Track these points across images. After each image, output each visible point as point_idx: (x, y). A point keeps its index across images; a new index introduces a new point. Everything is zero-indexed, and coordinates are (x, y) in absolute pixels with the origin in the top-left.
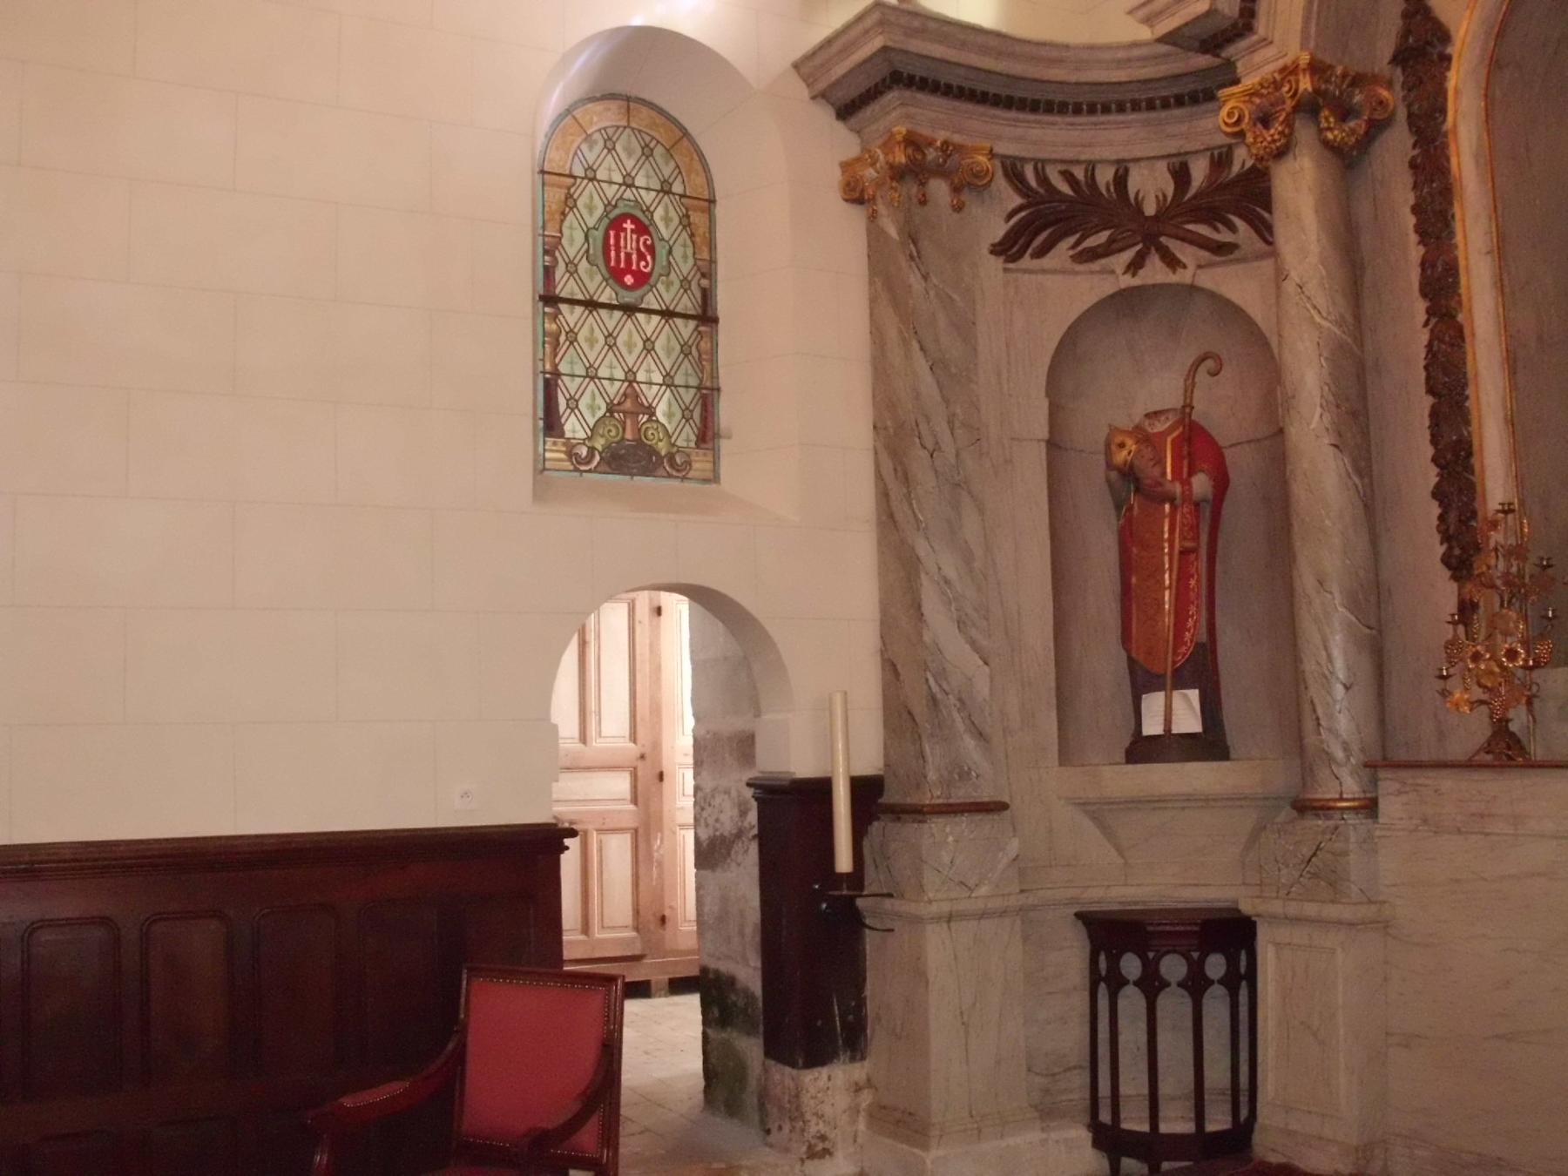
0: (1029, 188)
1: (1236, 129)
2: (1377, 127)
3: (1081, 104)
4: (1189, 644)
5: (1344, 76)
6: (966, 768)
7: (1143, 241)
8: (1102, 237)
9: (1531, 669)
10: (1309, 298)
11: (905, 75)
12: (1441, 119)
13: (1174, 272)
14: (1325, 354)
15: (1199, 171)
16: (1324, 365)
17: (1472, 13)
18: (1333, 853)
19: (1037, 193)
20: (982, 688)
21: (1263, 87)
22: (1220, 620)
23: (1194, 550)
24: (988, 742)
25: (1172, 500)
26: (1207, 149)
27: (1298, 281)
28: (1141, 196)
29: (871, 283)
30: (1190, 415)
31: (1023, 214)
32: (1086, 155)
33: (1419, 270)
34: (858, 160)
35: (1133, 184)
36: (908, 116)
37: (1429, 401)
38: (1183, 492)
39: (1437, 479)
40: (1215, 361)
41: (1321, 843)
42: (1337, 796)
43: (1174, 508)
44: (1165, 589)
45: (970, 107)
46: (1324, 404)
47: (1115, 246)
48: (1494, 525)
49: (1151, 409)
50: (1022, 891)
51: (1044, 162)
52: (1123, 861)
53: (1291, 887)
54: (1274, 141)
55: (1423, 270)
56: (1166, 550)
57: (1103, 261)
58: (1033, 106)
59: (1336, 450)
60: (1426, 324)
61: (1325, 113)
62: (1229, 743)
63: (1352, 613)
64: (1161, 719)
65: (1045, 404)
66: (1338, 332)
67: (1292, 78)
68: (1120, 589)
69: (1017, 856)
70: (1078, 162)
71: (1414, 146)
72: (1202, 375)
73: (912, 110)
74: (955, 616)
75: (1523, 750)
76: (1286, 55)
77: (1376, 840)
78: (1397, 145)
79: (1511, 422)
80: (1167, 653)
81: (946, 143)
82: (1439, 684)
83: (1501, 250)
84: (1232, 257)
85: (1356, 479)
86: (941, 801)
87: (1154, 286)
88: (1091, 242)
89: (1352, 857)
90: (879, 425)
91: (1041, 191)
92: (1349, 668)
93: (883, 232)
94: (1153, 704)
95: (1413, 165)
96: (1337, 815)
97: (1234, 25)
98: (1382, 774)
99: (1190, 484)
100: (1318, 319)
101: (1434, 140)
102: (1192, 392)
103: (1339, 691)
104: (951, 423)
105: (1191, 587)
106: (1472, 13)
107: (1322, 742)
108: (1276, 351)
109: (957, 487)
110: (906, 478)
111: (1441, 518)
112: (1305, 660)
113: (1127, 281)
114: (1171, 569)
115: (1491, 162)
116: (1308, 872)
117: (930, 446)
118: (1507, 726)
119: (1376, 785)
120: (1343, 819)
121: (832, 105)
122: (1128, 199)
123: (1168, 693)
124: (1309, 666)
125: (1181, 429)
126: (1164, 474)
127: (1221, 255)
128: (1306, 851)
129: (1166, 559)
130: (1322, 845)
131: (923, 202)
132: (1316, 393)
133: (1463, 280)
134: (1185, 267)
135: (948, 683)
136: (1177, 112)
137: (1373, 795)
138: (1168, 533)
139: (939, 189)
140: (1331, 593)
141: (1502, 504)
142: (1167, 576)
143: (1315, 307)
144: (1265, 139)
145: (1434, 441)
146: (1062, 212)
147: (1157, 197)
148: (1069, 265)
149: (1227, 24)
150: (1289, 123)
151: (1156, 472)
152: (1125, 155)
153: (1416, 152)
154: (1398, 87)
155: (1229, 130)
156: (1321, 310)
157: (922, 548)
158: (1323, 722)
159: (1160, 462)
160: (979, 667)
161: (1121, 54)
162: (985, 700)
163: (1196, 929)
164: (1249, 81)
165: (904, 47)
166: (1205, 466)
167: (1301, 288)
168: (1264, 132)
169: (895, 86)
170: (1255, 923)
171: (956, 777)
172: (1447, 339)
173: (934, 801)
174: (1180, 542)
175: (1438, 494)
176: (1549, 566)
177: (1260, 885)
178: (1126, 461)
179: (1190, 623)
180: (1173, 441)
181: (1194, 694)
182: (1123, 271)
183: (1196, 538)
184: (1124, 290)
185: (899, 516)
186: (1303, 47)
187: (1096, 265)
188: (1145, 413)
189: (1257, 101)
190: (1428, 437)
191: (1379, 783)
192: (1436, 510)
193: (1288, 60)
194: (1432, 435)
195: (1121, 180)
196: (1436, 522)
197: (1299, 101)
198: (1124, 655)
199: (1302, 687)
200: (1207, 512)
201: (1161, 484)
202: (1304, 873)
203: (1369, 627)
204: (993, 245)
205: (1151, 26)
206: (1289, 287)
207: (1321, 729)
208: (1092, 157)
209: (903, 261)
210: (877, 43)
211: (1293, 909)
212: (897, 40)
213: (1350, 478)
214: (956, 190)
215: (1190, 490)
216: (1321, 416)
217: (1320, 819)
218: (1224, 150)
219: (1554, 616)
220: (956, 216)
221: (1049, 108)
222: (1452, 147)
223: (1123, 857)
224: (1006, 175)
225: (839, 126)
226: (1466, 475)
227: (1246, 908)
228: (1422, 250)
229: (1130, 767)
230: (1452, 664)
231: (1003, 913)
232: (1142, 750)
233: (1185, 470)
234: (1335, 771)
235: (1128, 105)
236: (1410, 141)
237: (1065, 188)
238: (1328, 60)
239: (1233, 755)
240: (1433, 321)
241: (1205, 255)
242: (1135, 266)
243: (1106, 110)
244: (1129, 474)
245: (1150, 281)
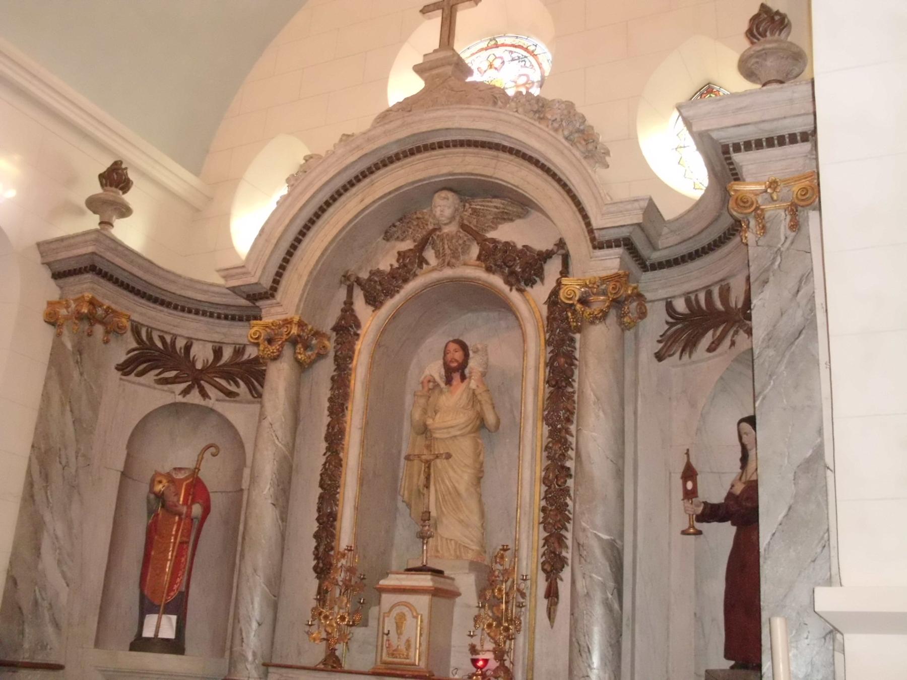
0: (142, 340)
1: (256, 341)
2: (320, 356)
3: (178, 305)
5: (311, 330)
6: (45, 643)
7: (192, 380)
8: (172, 374)
9: (351, 626)
10: (274, 431)
11: (98, 268)
12: (350, 361)
13: (204, 400)
14: (277, 459)
15: (227, 354)
17: (373, 318)
19: (145, 344)
20: (64, 597)
21: (273, 325)
23: (187, 543)
24: (60, 630)
25: (180, 515)
26: (234, 344)
28: (196, 358)
29: (49, 368)
30: (198, 473)
31: (136, 352)
32: (175, 331)
33: (326, 428)
34: (59, 303)
35: (193, 352)
36: (93, 289)
37: (320, 491)
38: (187, 512)
39: (317, 529)
43: (180, 519)
44: (168, 560)
45: (125, 292)
47: (179, 380)
48: (343, 555)
51: (152, 328)
54: (273, 352)
55: (328, 429)
56: (172, 540)
57: (169, 386)
58: (155, 300)
59: (273, 506)
60: (325, 454)
61: (299, 346)
64: (154, 629)
65: (125, 452)
67: (289, 325)
70: (169, 333)
71: (335, 371)
72: (207, 454)
73: (96, 286)
75: (340, 665)
76: (287, 313)
78: (326, 369)
79: (356, 508)
81: (109, 308)
82: (307, 629)
83: (366, 427)
84: (235, 399)
85: (280, 522)
86: (27, 661)
87: (192, 404)
88: (168, 375)
90: (35, 445)
91: (148, 343)
93: (63, 345)
94: (151, 621)
95: (332, 378)
97: (266, 293)
99: (191, 508)
100: (277, 442)
101: (345, 370)
103: (254, 625)
104: (77, 453)
106: (373, 318)
107: (243, 650)
109: (73, 487)
110: (46, 477)
111: (317, 548)
113: (180, 399)
114: (173, 551)
115: (369, 386)
117: (64, 463)
118: (334, 653)
121: (51, 270)
122: (189, 357)
125: (191, 479)
126: (179, 500)
127: (231, 397)
129: (172, 545)
131: (90, 335)
132: (270, 477)
133: (347, 437)
134: (210, 399)
135: (46, 594)
136: (224, 322)
138: (174, 532)
139: (99, 330)
140: (259, 576)
141: (348, 546)
142: (170, 554)
144: (269, 350)
145: (319, 510)
146: (155, 356)
147: (204, 361)
148: (153, 384)
149: (263, 291)
150: (282, 346)
151: (175, 499)
152: (193, 336)
153: (335, 373)
154: (333, 340)
155: (252, 341)
157: (47, 518)
158: (245, 640)
159: (177, 494)
161: (205, 287)
164: (267, 320)
165: (102, 254)
166: (201, 501)
167: (271, 425)
168: (269, 346)
169: (91, 272)
171: (39, 648)
172: (333, 463)
173: (24, 660)
174: (181, 537)
175: (317, 536)
176: (364, 579)
178: (160, 491)
179: (178, 580)
180: (187, 485)
181: (174, 618)
183: (189, 536)
184: (177, 403)
185: (38, 498)
186: (297, 311)
187: (166, 387)
189: (269, 331)
190: (316, 508)
191: (269, 674)
192: (314, 543)
193: (288, 316)
195: (188, 348)
196: (313, 549)
197: (290, 337)
199: (237, 621)
201: (176, 506)
204: (118, 365)
205: (226, 281)
206: (265, 423)
208: (176, 333)
209: (72, 363)
210: (90, 249)
212: (101, 250)
213: (278, 521)
214: (107, 332)
215: (191, 512)
216: (269, 489)
218: (242, 346)
219: (363, 602)
220: (104, 346)
221: (162, 303)
222: (353, 376)
224: (132, 330)
225: (52, 282)
226: (332, 529)
228: (329, 419)
230: (314, 620)
232: (140, 644)
235: (201, 312)
236: (334, 367)
237: (159, 344)
238: (306, 322)
240: (328, 454)
241: (221, 395)
242: (185, 392)
243: (190, 311)
244: (160, 496)
245: (191, 402)
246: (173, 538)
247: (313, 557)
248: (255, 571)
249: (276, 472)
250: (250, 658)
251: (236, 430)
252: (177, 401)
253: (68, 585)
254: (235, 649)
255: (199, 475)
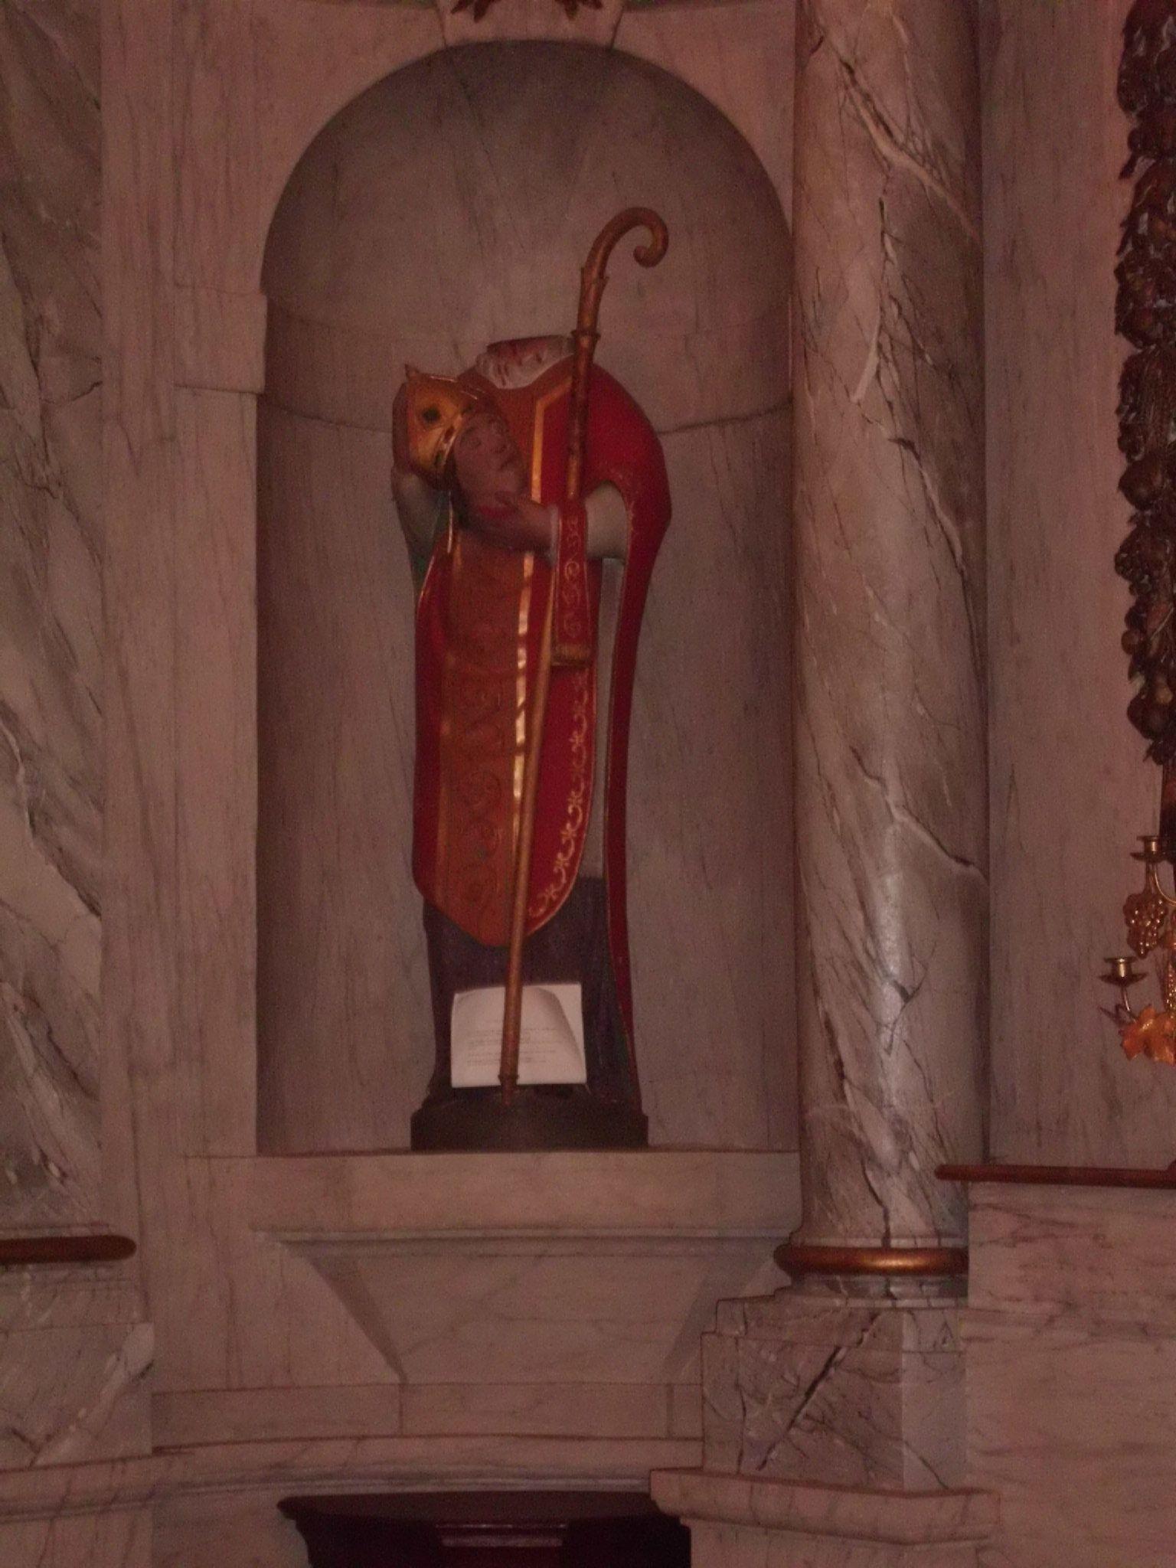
4: (564, 881)
6: (36, 1158)
10: (867, 98)
16: (892, 254)
18: (864, 1375)
22: (634, 829)
23: (588, 664)
25: (540, 548)
27: (847, 57)
33: (1120, 44)
37: (1122, 349)
40: (652, 229)
41: (838, 1349)
42: (877, 1243)
43: (543, 566)
46: (887, 348)
49: (506, 334)
50: (158, 1451)
52: (395, 1378)
53: (770, 1450)
55: (1129, 44)
56: (521, 664)
59: (907, 454)
60: (1126, 172)
62: (647, 1108)
63: (926, 828)
64: (494, 1049)
66: (927, 179)
68: (413, 745)
69: (149, 1367)
74: (25, 797)
77: (962, 1345)
80: (514, 895)
82: (1109, 995)
85: (948, 522)
89: (905, 1385)
92: (911, 949)
96: (875, 1284)
98: (981, 1193)
99: (582, 514)
100: (884, 147)
102: (598, 297)
103: (890, 1001)
105: (574, 749)
107: (845, 1115)
108: (788, 215)
111: (1136, 619)
112: (816, 930)
116: (807, 1416)
119: (964, 1222)
120: (889, 1295)
123: (513, 990)
124: (825, 943)
125: (568, 383)
126: (526, 483)
128: (806, 1364)
130: (840, 1356)
137: (958, 1243)
140: (879, 779)
142: (520, 723)
143: (879, 119)
145: (1128, 438)
151: (508, 482)
156: (892, 126)
158: (850, 1070)
159: (517, 459)
160: (77, 917)
162: (88, 996)
163: (555, 1542)
167: (851, 71)
170: (685, 1535)
174: (553, 644)
177: (703, 1439)
182: (452, 7)
183: (591, 639)
188: (488, 341)
190: (1114, 432)
192: (1122, 597)
194: (1125, 429)
198: (418, 899)
200: (617, 572)
202: (800, 1417)
203: (965, 862)
206: (825, 67)
207: (847, 1087)
211: (771, 1501)
217: (838, 1291)
223: (398, 1369)
227: (668, 1496)
229: (420, 1161)
231: (107, 1504)
233: (573, 482)
234: (875, 1185)
239: (656, 1134)
240: (1143, 164)
246: (522, 652)
247: (1125, 661)
248: (859, 755)
249: (902, 295)
250: (885, 1146)
251: (734, 131)
252: (452, 39)
253: (94, 909)
254: (814, 1112)
255: (600, 357)
